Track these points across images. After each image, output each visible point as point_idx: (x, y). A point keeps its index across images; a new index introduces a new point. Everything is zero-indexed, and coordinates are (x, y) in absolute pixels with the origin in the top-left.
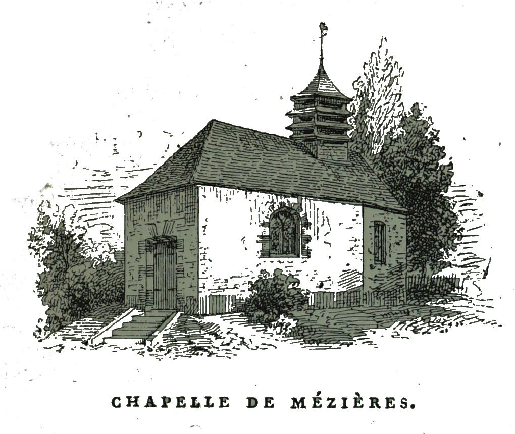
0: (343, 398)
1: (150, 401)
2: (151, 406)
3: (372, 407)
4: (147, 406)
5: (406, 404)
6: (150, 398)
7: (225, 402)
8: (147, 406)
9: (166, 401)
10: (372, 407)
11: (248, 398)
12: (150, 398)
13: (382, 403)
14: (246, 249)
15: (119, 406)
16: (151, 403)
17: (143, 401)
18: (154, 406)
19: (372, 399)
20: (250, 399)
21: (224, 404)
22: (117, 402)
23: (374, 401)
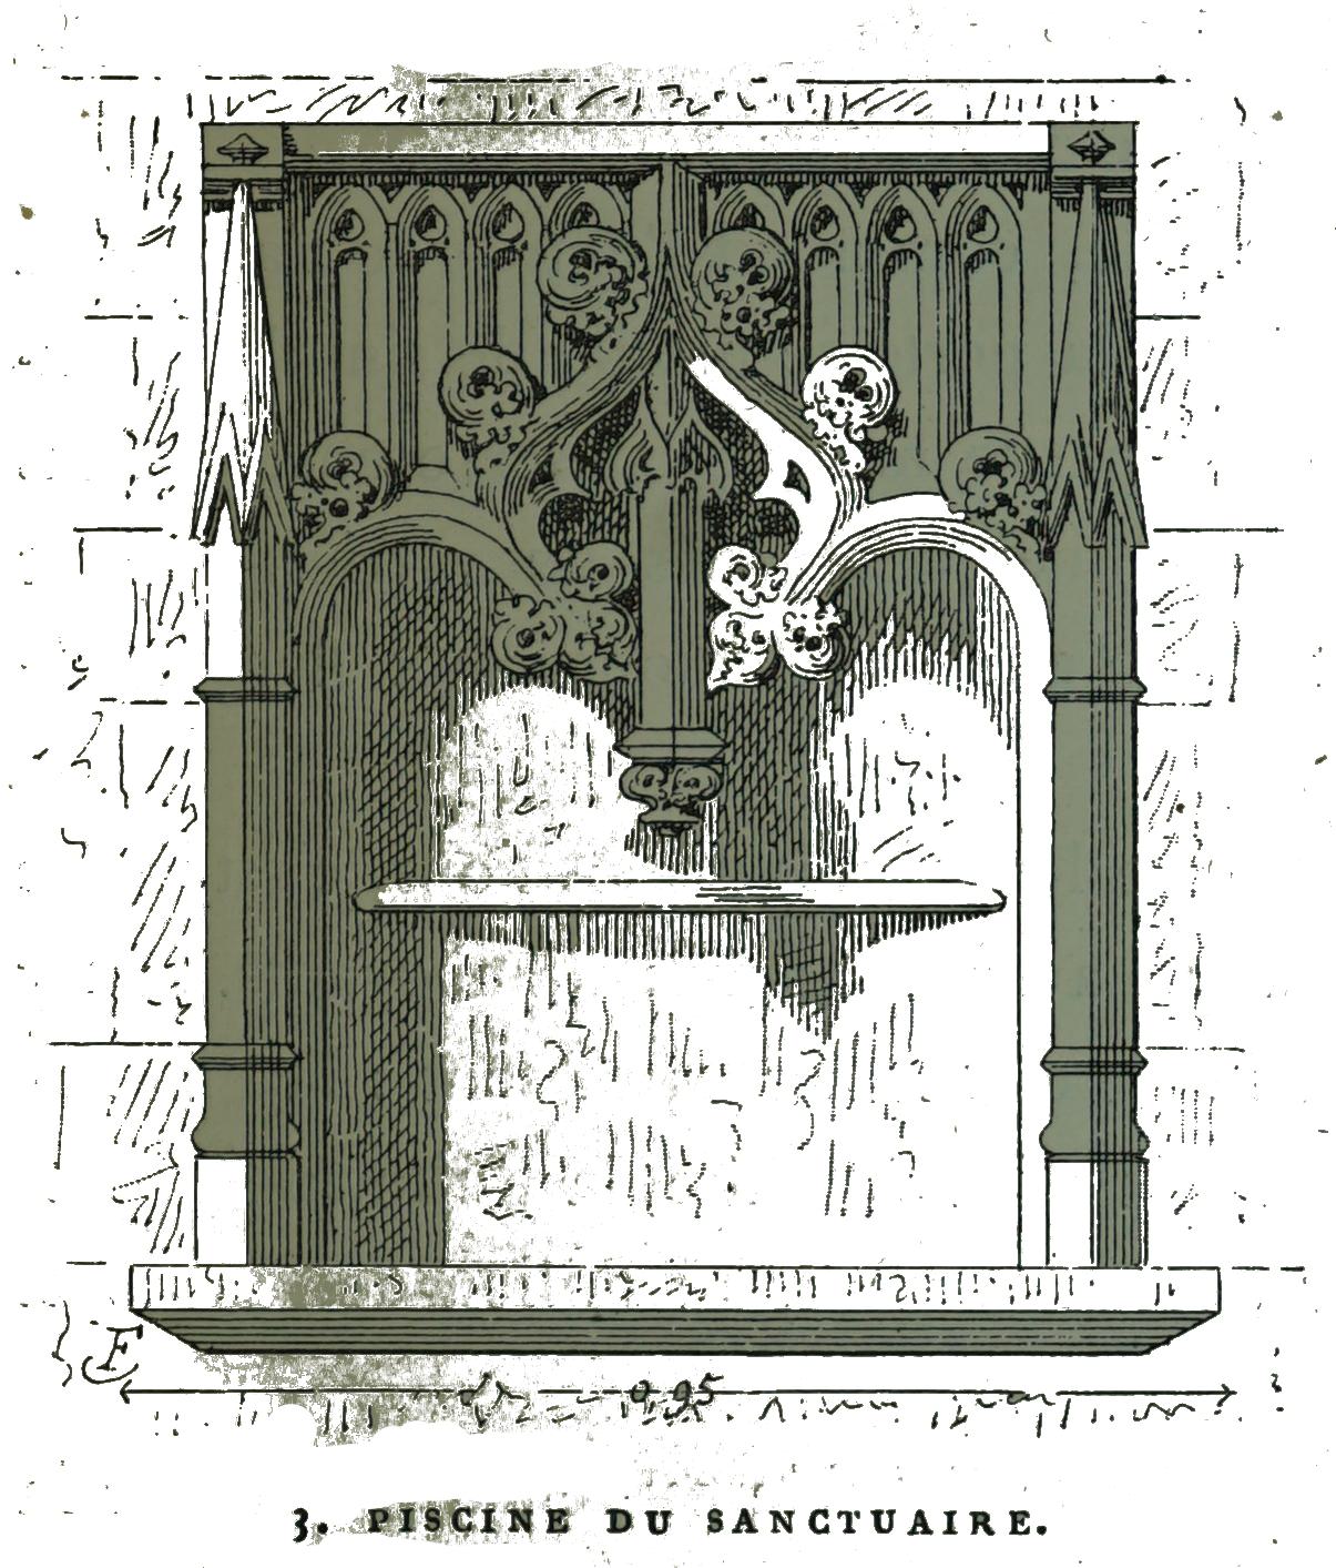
0: (873, 1512)
1: (919, 1521)
2: (923, 1533)
3: (513, 1529)
4: (913, 1532)
5: (720, 1523)
6: (920, 1514)
7: (1022, 1523)
8: (913, 1532)
9: (746, 1521)
10: (513, 1529)
11: (609, 1512)
12: (920, 1514)
13: (1001, 1522)
14: (94, 1323)
15: (826, 1530)
16: (921, 1524)
17: (904, 1521)
18: (927, 1531)
19: (974, 1515)
20: (613, 1513)
21: (1021, 1528)
22: (820, 1522)
23: (980, 1519)
